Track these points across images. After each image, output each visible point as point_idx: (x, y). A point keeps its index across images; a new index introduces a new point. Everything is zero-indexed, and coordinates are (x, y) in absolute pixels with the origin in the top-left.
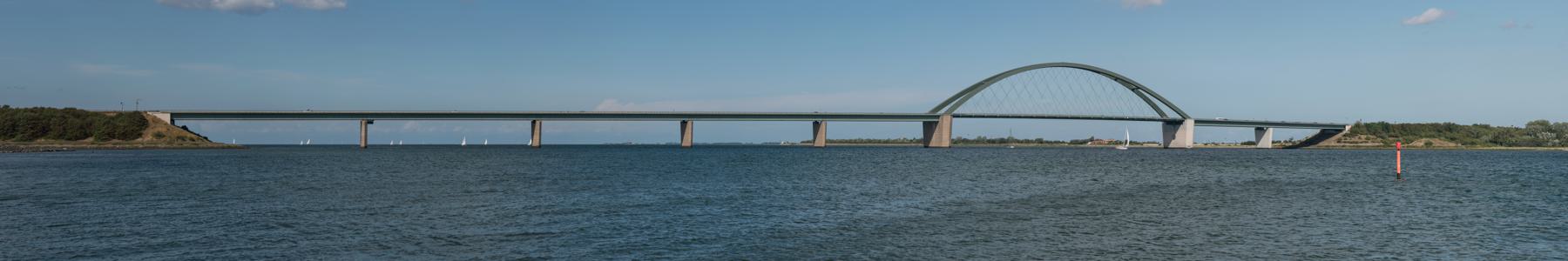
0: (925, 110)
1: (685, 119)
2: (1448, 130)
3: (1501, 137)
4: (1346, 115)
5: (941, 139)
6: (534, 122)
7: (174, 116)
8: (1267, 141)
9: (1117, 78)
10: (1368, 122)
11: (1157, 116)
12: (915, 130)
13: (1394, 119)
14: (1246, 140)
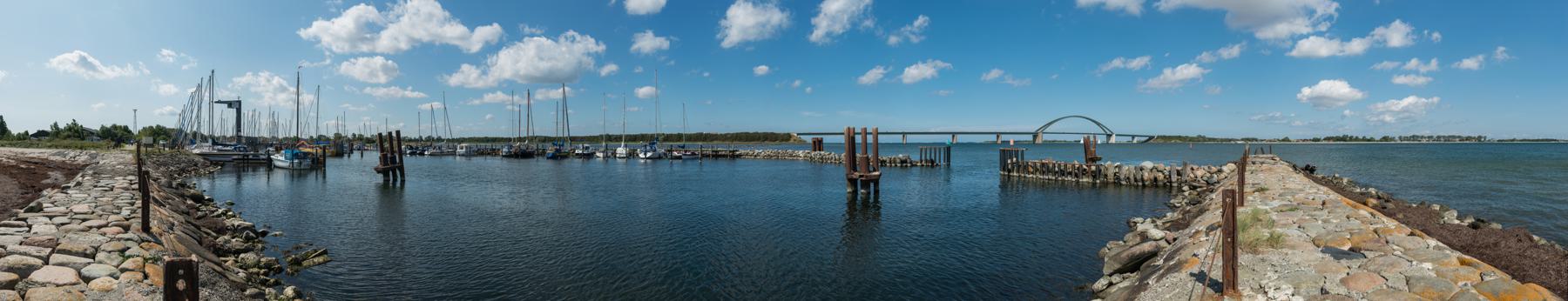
0: (1034, 131)
1: (954, 134)
2: (1179, 138)
3: (1192, 139)
4: (1155, 133)
5: (1039, 141)
6: (953, 136)
7: (798, 134)
8: (1135, 141)
9: (1090, 120)
10: (610, 134)
11: (1103, 132)
12: (1030, 138)
13: (1167, 135)
14: (1244, 137)
